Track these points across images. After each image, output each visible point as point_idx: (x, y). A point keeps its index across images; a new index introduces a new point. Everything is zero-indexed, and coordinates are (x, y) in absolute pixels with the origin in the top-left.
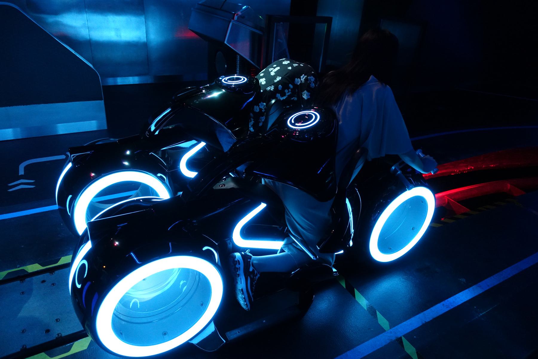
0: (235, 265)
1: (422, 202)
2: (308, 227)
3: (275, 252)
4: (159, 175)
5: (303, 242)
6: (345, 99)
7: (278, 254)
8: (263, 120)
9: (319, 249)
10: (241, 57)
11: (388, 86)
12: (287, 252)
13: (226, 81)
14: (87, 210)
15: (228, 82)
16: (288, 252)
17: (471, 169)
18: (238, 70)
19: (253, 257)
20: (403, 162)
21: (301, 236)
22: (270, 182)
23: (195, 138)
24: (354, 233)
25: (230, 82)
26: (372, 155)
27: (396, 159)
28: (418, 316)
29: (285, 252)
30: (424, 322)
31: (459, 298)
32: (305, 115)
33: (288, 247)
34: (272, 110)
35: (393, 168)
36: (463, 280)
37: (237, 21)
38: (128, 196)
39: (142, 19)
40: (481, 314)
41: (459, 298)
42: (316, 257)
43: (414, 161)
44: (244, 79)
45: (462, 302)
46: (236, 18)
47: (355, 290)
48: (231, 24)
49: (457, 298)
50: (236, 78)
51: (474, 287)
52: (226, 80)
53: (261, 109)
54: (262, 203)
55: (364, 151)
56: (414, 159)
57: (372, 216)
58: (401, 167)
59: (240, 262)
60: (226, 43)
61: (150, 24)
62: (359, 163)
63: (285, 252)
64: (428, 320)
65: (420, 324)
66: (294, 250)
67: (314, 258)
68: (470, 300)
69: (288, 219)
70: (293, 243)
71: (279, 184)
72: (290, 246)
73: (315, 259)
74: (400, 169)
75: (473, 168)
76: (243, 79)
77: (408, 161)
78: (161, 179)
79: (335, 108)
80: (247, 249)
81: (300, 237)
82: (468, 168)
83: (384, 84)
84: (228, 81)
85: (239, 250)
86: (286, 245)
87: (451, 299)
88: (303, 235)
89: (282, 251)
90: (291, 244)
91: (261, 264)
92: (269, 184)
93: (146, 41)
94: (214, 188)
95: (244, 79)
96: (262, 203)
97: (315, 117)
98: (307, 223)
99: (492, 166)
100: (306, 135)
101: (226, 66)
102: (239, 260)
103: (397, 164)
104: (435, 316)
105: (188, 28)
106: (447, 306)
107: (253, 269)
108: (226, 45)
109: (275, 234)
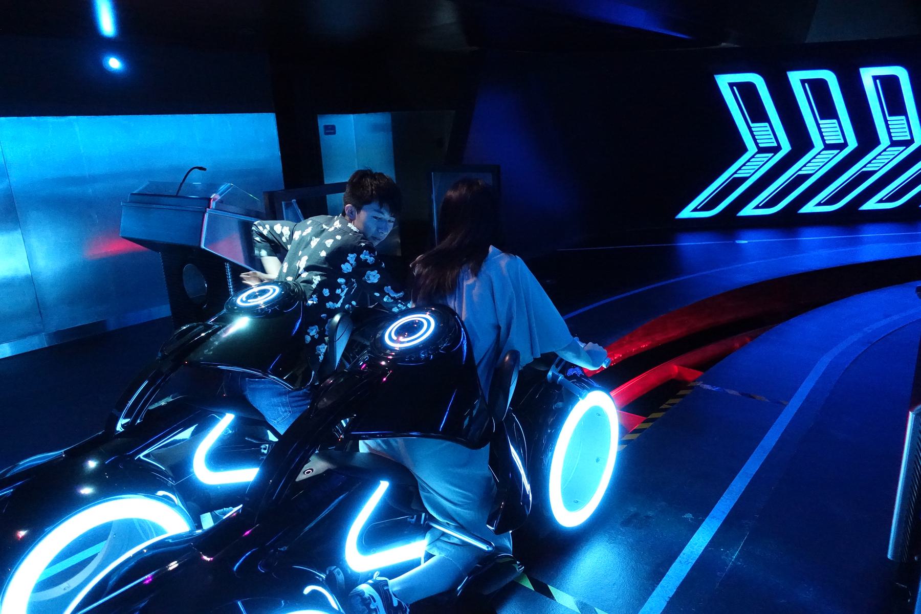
0: (368, 605)
1: (599, 415)
2: (462, 500)
3: (415, 564)
4: (161, 493)
5: (461, 528)
6: (463, 284)
7: (424, 565)
8: (324, 351)
9: (493, 528)
10: (232, 263)
11: (517, 256)
12: (438, 555)
13: (246, 302)
14: (581, 421)
15: (250, 302)
16: (440, 554)
17: (619, 357)
18: (231, 286)
19: (391, 582)
20: (562, 360)
21: (453, 520)
22: (379, 445)
23: (214, 410)
24: (531, 492)
25: (253, 302)
26: (526, 358)
27: (549, 359)
28: (654, 593)
29: (433, 556)
30: (668, 600)
31: (696, 544)
32: (413, 322)
33: (436, 546)
34: (339, 332)
35: (550, 374)
36: (689, 516)
37: (215, 209)
38: (89, 558)
39: (17, 236)
40: (734, 557)
41: (696, 544)
42: (490, 545)
43: (578, 356)
44: (274, 290)
45: (703, 548)
46: (213, 204)
47: (549, 586)
48: (207, 216)
49: (693, 545)
50: (259, 291)
51: (707, 520)
52: (244, 299)
53: (312, 337)
54: (381, 482)
55: (515, 355)
56: (578, 353)
57: (543, 459)
58: (559, 368)
59: (374, 597)
60: (204, 247)
61: (34, 242)
62: (513, 378)
63: (433, 556)
64: (671, 594)
65: (665, 604)
66: (448, 547)
67: (488, 548)
68: (711, 542)
69: (427, 499)
70: (441, 536)
71: (398, 442)
72: (439, 544)
73: (490, 549)
74: (560, 372)
75: (621, 356)
76: (271, 291)
77: (570, 358)
78: (165, 499)
79: (452, 304)
80: (373, 573)
81: (451, 522)
82: (615, 358)
83: (211, 339)
84: (249, 301)
85: (366, 578)
86: (432, 543)
87: (687, 550)
88: (457, 519)
89: (429, 556)
90: (438, 539)
91: (405, 591)
92: (379, 449)
93: (30, 273)
94: (297, 480)
95: (274, 290)
96: (381, 482)
97: (428, 324)
98: (460, 493)
99: (644, 346)
100: (423, 353)
101: (206, 285)
102: (370, 594)
103: (553, 366)
104: (678, 583)
105: (120, 235)
106: (687, 563)
107: (398, 601)
108: (204, 250)
109: (406, 532)
